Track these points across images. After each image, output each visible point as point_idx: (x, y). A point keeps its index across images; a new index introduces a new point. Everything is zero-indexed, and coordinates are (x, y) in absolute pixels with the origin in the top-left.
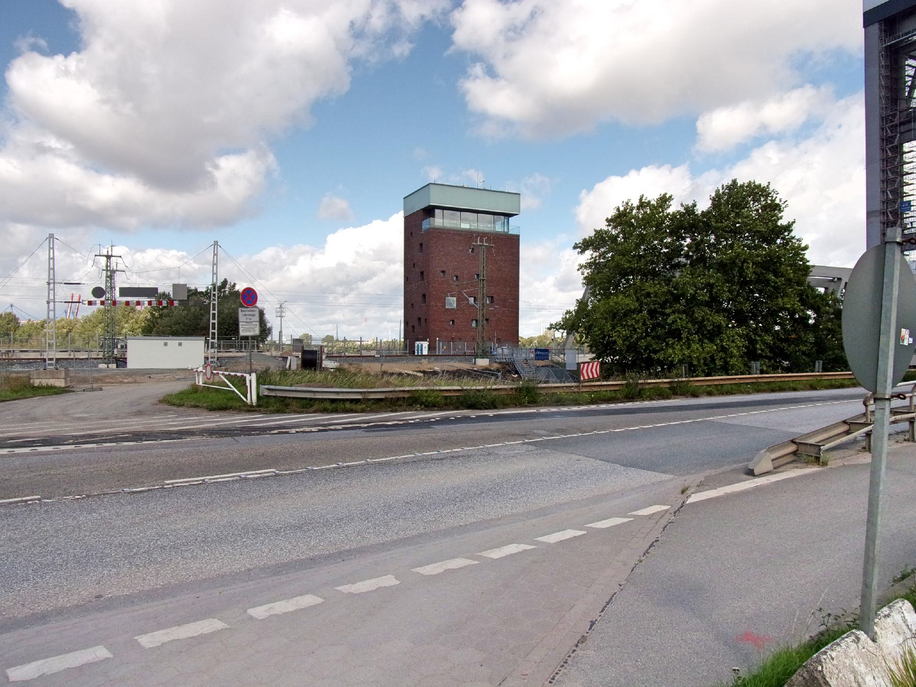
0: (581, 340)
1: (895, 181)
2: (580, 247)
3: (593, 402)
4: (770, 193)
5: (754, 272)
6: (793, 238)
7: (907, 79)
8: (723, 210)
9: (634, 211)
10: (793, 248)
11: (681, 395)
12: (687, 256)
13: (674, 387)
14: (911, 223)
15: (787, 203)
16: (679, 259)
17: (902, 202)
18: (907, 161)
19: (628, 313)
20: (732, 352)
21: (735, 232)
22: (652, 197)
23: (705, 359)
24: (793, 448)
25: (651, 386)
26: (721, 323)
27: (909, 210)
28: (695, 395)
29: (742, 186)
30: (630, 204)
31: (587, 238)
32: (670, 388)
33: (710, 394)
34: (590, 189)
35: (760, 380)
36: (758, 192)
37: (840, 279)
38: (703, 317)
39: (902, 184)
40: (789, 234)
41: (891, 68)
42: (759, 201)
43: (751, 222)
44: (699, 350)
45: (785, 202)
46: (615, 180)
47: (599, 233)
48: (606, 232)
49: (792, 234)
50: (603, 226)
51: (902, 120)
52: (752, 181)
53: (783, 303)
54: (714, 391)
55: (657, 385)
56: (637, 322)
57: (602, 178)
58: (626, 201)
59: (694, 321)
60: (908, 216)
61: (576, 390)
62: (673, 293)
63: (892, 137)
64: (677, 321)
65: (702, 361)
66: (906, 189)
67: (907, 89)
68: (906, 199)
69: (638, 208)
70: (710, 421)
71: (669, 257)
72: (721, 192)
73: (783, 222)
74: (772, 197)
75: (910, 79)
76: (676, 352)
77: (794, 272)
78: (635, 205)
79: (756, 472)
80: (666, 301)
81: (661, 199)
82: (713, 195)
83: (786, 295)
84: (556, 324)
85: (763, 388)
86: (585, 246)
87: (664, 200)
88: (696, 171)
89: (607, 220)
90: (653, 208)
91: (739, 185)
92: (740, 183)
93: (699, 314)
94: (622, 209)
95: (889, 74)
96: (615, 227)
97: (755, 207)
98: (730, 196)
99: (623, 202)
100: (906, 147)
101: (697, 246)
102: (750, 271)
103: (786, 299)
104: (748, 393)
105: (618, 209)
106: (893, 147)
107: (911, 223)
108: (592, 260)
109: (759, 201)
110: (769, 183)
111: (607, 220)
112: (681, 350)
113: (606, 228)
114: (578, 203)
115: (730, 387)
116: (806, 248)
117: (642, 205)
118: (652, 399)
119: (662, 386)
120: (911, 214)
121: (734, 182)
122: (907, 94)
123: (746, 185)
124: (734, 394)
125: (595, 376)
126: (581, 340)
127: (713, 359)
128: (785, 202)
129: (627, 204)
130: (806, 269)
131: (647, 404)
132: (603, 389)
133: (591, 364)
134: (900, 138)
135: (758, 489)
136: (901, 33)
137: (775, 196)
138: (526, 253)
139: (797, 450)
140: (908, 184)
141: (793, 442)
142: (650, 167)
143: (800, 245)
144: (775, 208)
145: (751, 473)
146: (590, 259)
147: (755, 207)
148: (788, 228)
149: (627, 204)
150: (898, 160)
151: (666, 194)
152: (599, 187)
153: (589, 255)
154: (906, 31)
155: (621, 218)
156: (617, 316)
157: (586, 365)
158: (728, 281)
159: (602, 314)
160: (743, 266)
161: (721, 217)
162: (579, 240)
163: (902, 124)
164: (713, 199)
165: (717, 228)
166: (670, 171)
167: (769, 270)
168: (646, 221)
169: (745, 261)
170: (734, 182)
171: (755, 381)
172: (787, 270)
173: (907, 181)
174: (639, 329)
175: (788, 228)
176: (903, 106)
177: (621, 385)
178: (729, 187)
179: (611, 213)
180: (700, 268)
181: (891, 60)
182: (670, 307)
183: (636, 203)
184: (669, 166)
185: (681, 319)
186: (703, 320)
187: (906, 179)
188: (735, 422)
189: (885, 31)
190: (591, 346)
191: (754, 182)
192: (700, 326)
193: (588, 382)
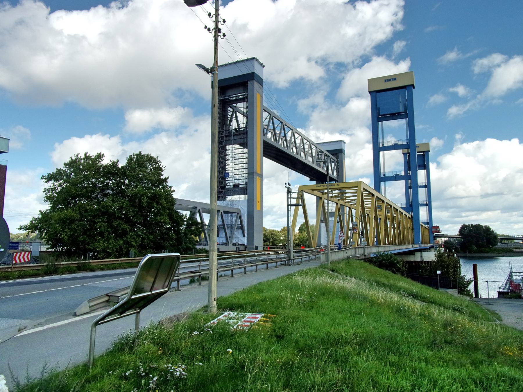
0: (41, 237)
1: (222, 162)
2: (45, 179)
3: (19, 278)
4: (158, 162)
5: (146, 202)
6: (168, 186)
7: (229, 116)
8: (133, 166)
9: (82, 161)
10: (167, 191)
11: (83, 270)
12: (112, 190)
13: (80, 266)
14: (229, 183)
15: (165, 168)
16: (108, 191)
17: (225, 173)
18: (228, 154)
19: (72, 221)
20: (132, 244)
21: (140, 180)
22: (93, 154)
23: (116, 249)
24: (106, 298)
25: (65, 266)
26: (126, 229)
27: (228, 177)
28: (92, 270)
29: (144, 156)
30: (79, 156)
31: (51, 173)
32: (76, 267)
33: (102, 269)
34: (61, 142)
35: (133, 261)
36: (151, 160)
37: (196, 207)
38: (117, 225)
39: (226, 165)
40: (166, 183)
41: (222, 110)
42: (152, 164)
43: (147, 174)
44: (113, 243)
45: (164, 167)
46: (76, 140)
47: (59, 170)
48: (64, 171)
49: (167, 184)
50: (62, 167)
51: (226, 135)
52: (149, 154)
53: (160, 218)
54: (106, 268)
55: (67, 265)
56: (78, 226)
57: (68, 138)
58: (76, 154)
59: (112, 227)
60: (228, 179)
61: (9, 270)
62: (101, 210)
63: (222, 142)
64: (101, 227)
65: (115, 250)
66: (227, 167)
67: (229, 121)
68: (227, 172)
69: (84, 159)
70: (87, 286)
71: (102, 189)
72: (133, 156)
73: (163, 177)
74: (159, 164)
75: (230, 117)
76: (100, 245)
77: (167, 203)
78: (82, 158)
79: (77, 314)
80: (97, 215)
81: (97, 155)
82: (129, 157)
83: (162, 215)
84: (24, 226)
85: (135, 265)
86: (50, 178)
87: (100, 157)
88: (125, 141)
89: (65, 164)
90: (93, 160)
91: (142, 155)
92: (143, 153)
93: (115, 223)
94: (74, 158)
95: (221, 112)
96: (70, 169)
97: (150, 167)
98: (137, 159)
99: (75, 155)
100: (228, 147)
101: (118, 184)
102: (145, 201)
103: (161, 217)
104: (125, 268)
105: (72, 158)
106: (222, 146)
107: (229, 183)
108: (53, 187)
109: (152, 164)
110: (158, 157)
111: (65, 164)
112: (103, 244)
113: (64, 169)
114: (54, 150)
115: (116, 264)
116: (174, 191)
117: (87, 158)
118: (63, 274)
119: (71, 266)
120: (229, 179)
121: (140, 153)
122: (228, 123)
123: (146, 155)
124: (117, 269)
125: (27, 260)
126: (41, 237)
127: (121, 248)
128: (164, 167)
129: (77, 156)
130: (173, 201)
131: (58, 277)
132: (30, 269)
133: (23, 253)
134: (225, 143)
135: (76, 322)
136: (226, 95)
137: (160, 164)
138: (9, 175)
139: (109, 300)
140: (228, 165)
141: (107, 295)
142: (97, 135)
143: (171, 189)
144: (159, 170)
145: (75, 315)
146: (53, 186)
147: (150, 167)
148: (165, 180)
149: (77, 156)
150: (224, 153)
151: (101, 153)
152: (66, 142)
153: (51, 184)
154: (229, 94)
155: (73, 164)
156: (66, 222)
157: (27, 253)
158: (132, 206)
159: (56, 221)
160: (141, 198)
161: (133, 170)
162: (46, 174)
163: (226, 136)
164: (129, 160)
165: (129, 175)
166: (110, 139)
167: (155, 201)
168: (89, 168)
169: (142, 195)
170: (140, 153)
171: (130, 261)
172: (163, 202)
173: (228, 163)
174: (79, 230)
175: (165, 180)
176: (227, 128)
177: (43, 266)
178: (137, 155)
179: (67, 160)
180: (119, 197)
181: (222, 106)
182: (99, 218)
183: (83, 156)
184: (108, 136)
185: (104, 226)
186: (117, 227)
187: (228, 162)
188: (101, 285)
189: (220, 92)
190: (47, 241)
191: (150, 155)
192: (115, 230)
193: (20, 264)
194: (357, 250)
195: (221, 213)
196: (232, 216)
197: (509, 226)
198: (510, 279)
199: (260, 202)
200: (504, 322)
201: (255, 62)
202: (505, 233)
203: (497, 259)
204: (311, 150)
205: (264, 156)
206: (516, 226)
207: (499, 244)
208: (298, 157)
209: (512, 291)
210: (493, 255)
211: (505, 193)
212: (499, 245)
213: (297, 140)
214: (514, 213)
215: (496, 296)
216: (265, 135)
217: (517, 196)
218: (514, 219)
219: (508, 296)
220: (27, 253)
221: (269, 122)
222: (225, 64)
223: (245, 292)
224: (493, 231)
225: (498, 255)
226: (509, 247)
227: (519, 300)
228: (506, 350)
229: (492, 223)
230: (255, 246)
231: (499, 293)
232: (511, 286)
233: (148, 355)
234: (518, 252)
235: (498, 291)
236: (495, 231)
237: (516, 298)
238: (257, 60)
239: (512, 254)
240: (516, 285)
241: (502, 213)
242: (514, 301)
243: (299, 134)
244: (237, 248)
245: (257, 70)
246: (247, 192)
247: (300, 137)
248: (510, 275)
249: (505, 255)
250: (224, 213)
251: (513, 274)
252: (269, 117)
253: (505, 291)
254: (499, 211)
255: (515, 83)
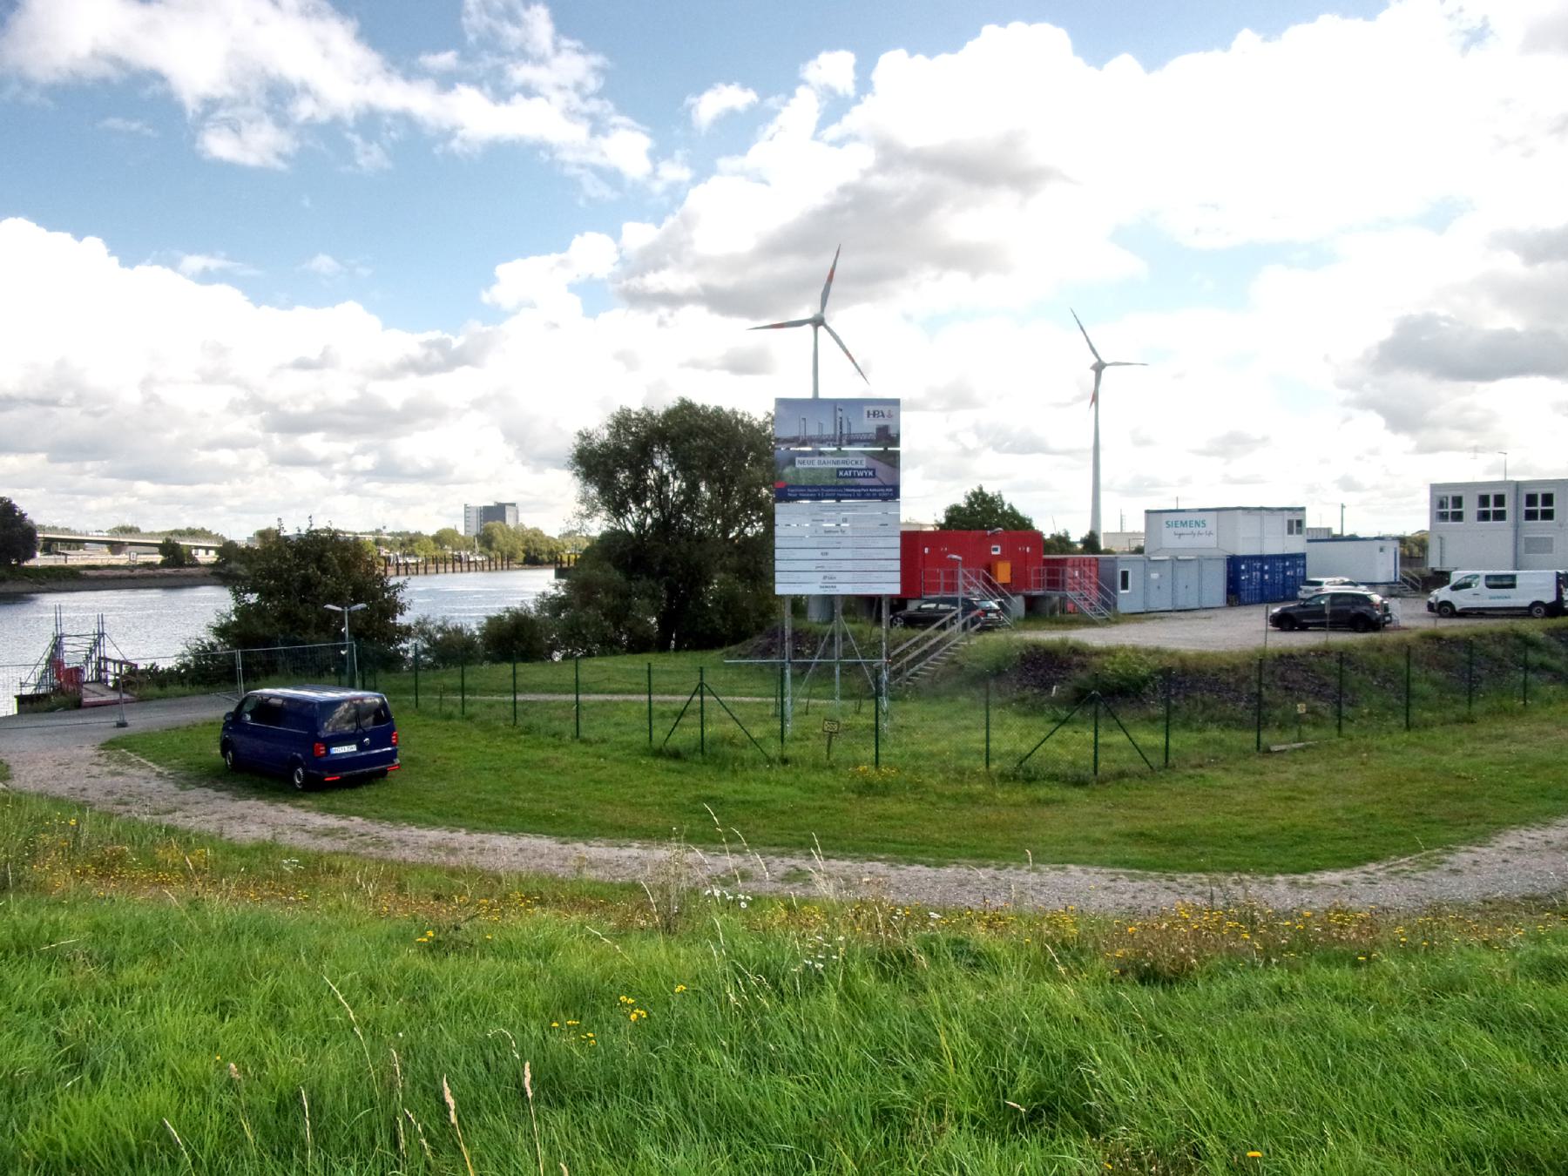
196: (1108, 746)
197: (72, 503)
198: (54, 661)
200: (15, 784)
202: (60, 523)
203: (32, 599)
206: (93, 504)
207: (38, 554)
209: (58, 690)
210: (19, 587)
211: (64, 401)
212: (40, 560)
214: (89, 465)
215: (12, 709)
217: (97, 415)
218: (87, 481)
219: (46, 705)
223: (63, 1006)
224: (23, 516)
225: (35, 587)
226: (70, 563)
227: (80, 712)
228: (1396, 826)
229: (21, 493)
231: (22, 700)
232: (58, 677)
233: (1394, 981)
234: (97, 578)
235: (18, 693)
236: (28, 517)
237: (67, 709)
239: (78, 585)
240: (71, 670)
241: (51, 460)
242: (60, 718)
248: (57, 646)
249: (55, 586)
251: (65, 640)
253: (41, 691)
254: (43, 456)
255: (94, 54)
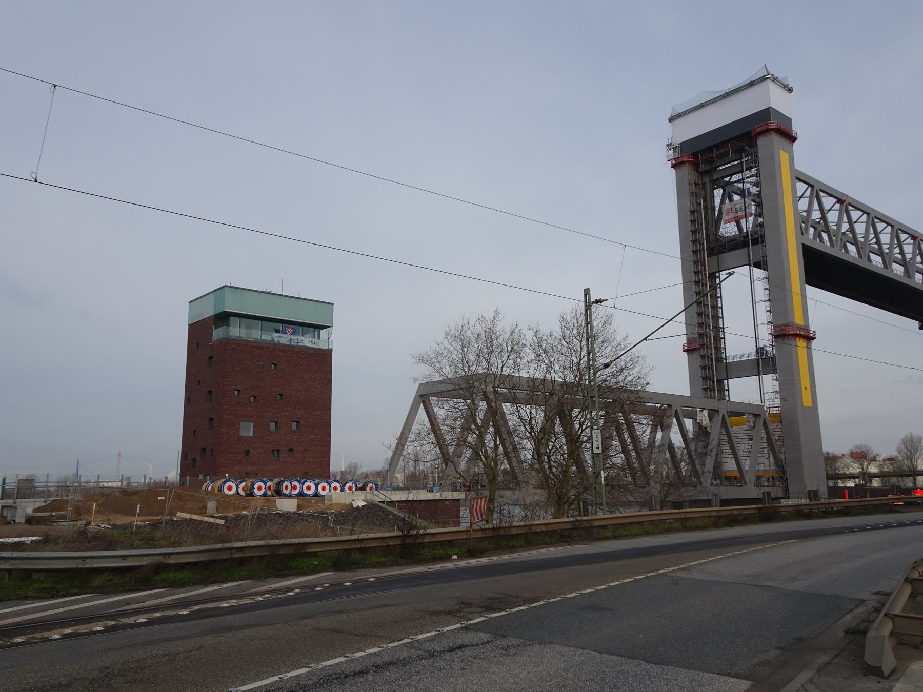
194: (299, 341)
195: (723, 415)
199: (809, 388)
201: (770, 85)
204: (900, 245)
205: (808, 283)
208: (863, 263)
213: (881, 236)
215: (23, 521)
216: (889, 268)
220: (483, 499)
221: (810, 204)
222: (699, 104)
230: (808, 491)
238: (775, 80)
243: (908, 233)
244: (763, 493)
245: (777, 100)
246: (774, 365)
247: (889, 227)
250: (729, 417)
252: (808, 193)
